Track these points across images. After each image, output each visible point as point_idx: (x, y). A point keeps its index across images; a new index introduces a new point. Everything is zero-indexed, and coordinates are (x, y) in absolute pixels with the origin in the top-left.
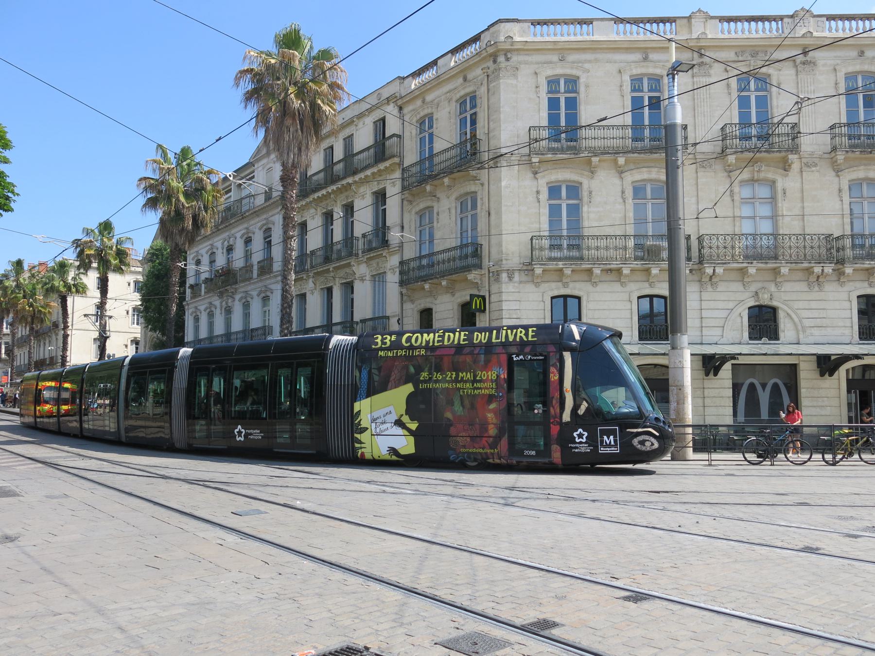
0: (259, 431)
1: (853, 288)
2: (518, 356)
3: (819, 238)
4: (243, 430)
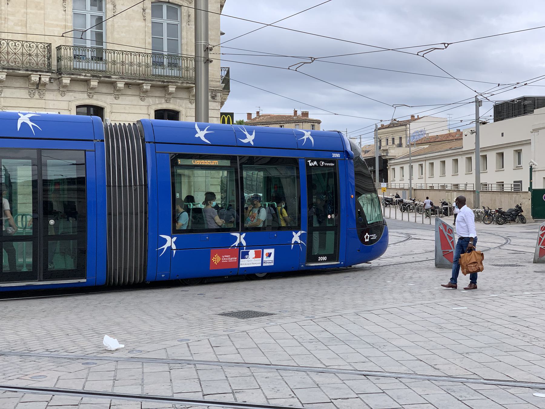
0: (375, 235)
1: (73, 99)
2: (312, 161)
3: (37, 47)
4: (368, 236)
